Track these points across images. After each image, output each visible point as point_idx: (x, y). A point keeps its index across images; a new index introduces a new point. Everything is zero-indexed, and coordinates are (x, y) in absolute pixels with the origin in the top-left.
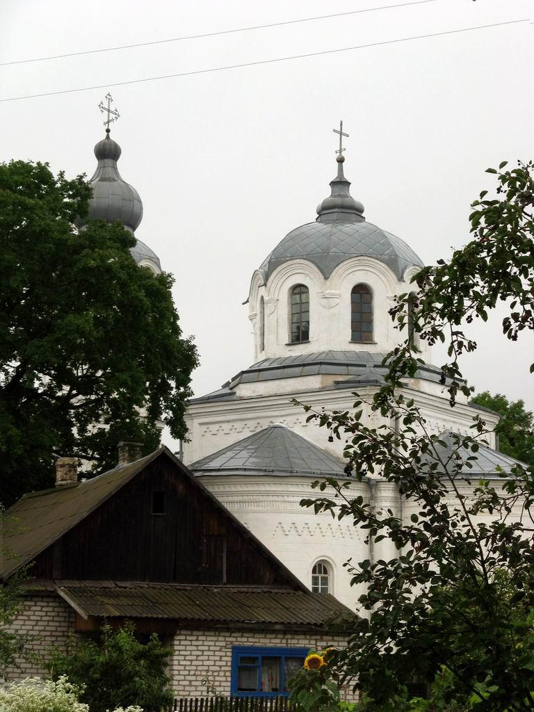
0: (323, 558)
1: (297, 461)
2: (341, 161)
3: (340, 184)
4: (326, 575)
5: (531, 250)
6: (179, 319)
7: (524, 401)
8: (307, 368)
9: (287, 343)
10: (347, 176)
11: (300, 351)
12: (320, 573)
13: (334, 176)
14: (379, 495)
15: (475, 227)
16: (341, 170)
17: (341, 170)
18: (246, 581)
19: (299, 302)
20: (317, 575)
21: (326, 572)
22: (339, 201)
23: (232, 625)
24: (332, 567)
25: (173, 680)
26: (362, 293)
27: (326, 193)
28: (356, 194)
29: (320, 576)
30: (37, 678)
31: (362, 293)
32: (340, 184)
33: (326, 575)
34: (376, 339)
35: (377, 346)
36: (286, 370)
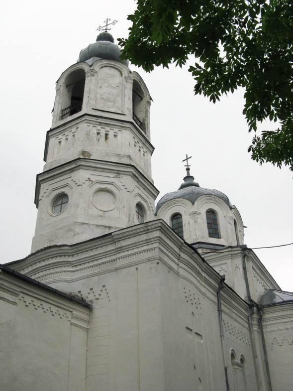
2: (188, 169)
3: (189, 177)
16: (188, 173)
17: (188, 173)
32: (189, 177)
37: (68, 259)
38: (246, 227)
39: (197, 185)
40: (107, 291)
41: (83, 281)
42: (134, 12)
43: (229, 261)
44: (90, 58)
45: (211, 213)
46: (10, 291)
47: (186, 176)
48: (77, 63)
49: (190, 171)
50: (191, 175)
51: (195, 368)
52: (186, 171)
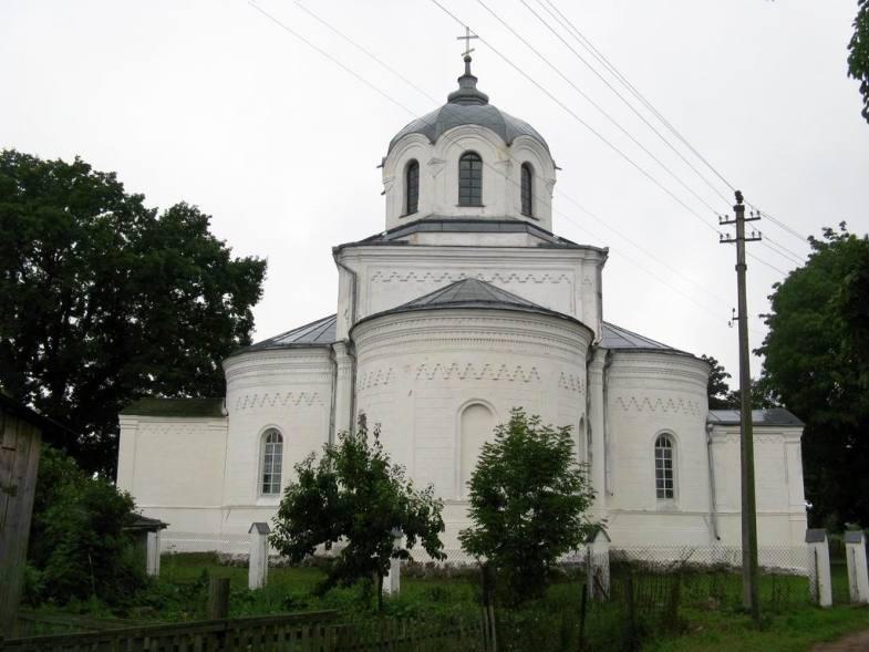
2: (468, 60)
3: (467, 79)
5: (53, 395)
6: (443, 530)
10: (473, 73)
11: (413, 218)
12: (664, 445)
13: (462, 72)
15: (715, 640)
16: (468, 68)
17: (468, 68)
18: (161, 562)
21: (669, 445)
22: (466, 92)
26: (471, 160)
27: (455, 87)
28: (481, 87)
30: (316, 465)
31: (471, 160)
32: (467, 79)
34: (484, 203)
35: (485, 209)
39: (483, 100)
43: (578, 267)
45: (527, 169)
49: (471, 64)
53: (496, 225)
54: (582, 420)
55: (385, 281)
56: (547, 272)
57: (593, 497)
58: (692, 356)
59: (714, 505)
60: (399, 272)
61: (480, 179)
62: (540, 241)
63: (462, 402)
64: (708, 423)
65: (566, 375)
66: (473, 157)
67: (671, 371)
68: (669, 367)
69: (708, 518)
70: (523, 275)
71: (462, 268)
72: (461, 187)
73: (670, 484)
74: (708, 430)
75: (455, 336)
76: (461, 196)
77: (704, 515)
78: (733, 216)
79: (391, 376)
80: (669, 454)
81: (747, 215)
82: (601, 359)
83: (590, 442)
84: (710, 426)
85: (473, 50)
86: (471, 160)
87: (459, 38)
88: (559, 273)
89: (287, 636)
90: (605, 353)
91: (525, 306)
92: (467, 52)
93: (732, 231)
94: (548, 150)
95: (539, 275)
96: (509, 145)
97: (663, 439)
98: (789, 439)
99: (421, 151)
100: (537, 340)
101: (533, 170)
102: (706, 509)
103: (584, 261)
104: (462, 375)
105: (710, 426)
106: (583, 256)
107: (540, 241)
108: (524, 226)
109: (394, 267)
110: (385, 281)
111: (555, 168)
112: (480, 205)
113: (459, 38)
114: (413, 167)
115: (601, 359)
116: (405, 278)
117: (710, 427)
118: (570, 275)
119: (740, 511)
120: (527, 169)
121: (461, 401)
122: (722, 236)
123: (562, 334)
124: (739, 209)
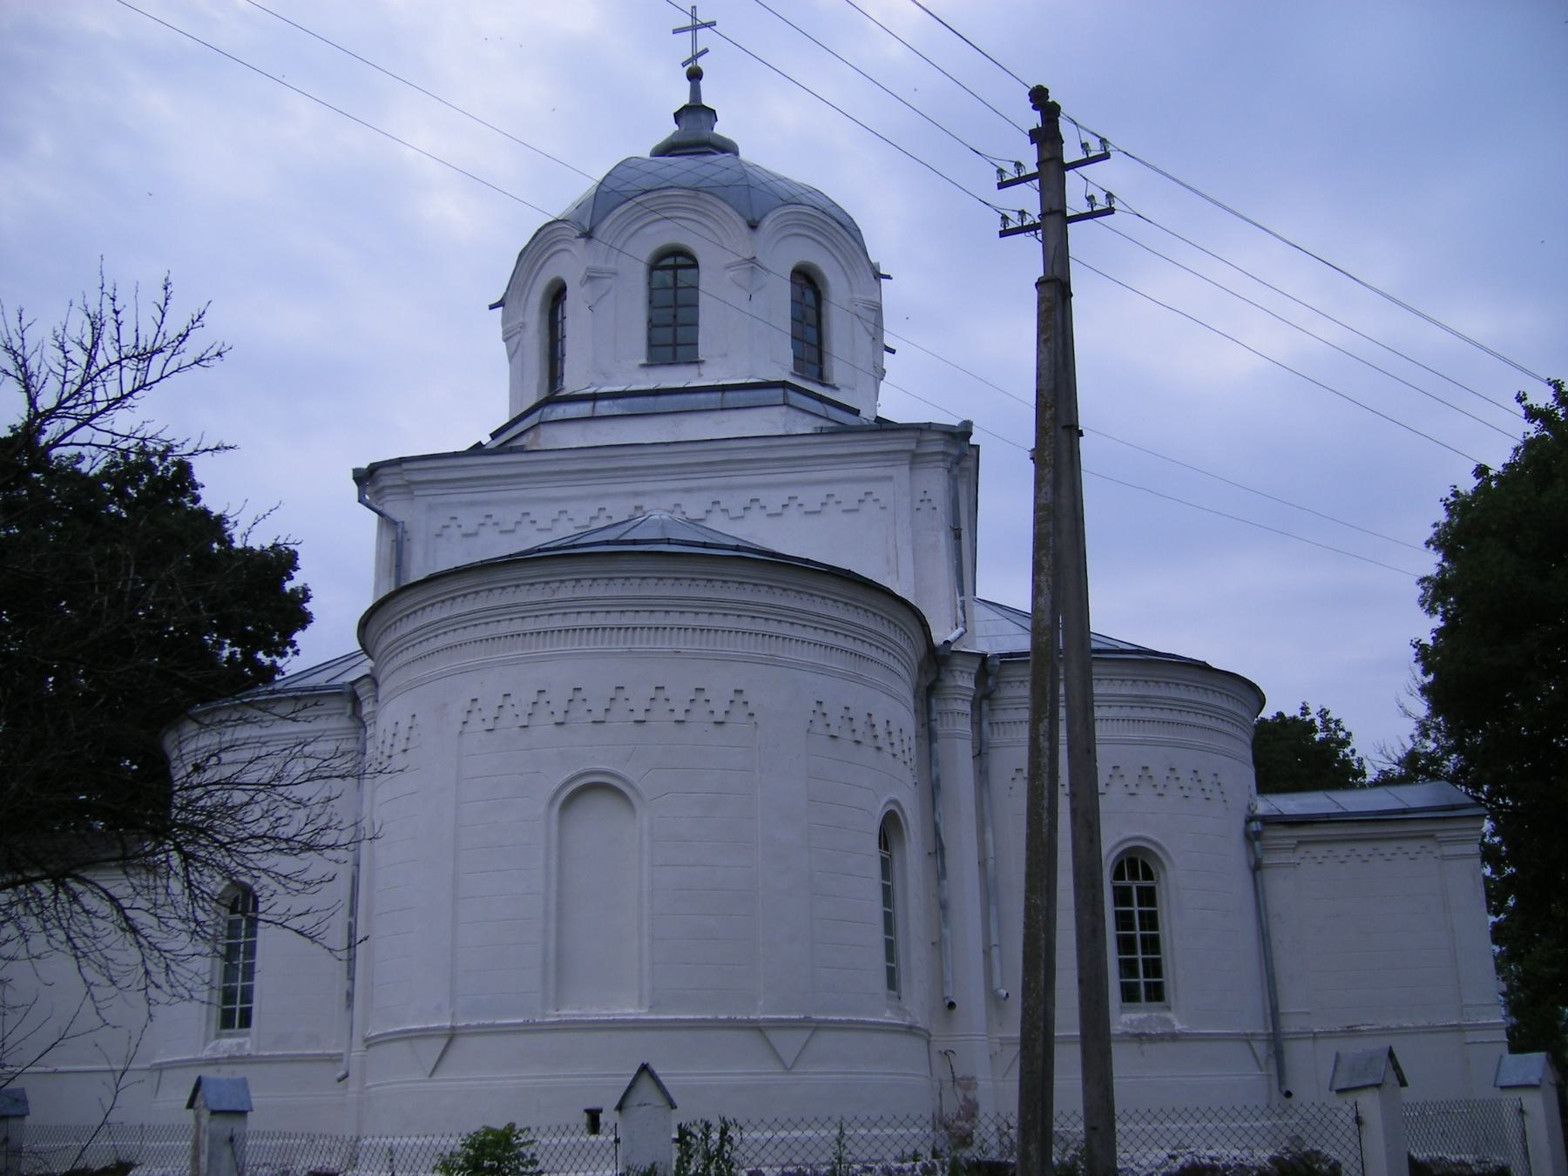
0: (1126, 846)
1: (625, 188)
2: (695, 76)
3: (695, 112)
4: (1148, 883)
7: (309, 586)
8: (729, 395)
9: (644, 361)
10: (706, 101)
12: (1134, 876)
13: (685, 100)
14: (949, 682)
16: (695, 92)
17: (695, 92)
19: (670, 350)
20: (1127, 882)
21: (1148, 875)
23: (220, 1061)
24: (1157, 857)
25: (148, 874)
29: (1134, 885)
32: (695, 112)
33: (1148, 883)
36: (651, 386)
37: (577, 620)
38: (893, 351)
39: (726, 147)
40: (750, 709)
41: (536, 448)
42: (216, 511)
43: (901, 472)
44: (414, 583)
45: (807, 281)
46: (510, 1031)
47: (686, 101)
48: (478, 449)
49: (704, 84)
50: (706, 102)
51: (901, 730)
52: (688, 84)
53: (716, 396)
54: (890, 829)
55: (466, 535)
56: (829, 489)
57: (142, 1126)
58: (1204, 667)
59: (1274, 1014)
60: (497, 513)
61: (694, 305)
62: (821, 423)
63: (561, 780)
64: (1250, 819)
65: (879, 721)
66: (680, 260)
67: (1143, 701)
68: (1140, 690)
69: (1261, 1048)
70: (775, 499)
71: (636, 494)
72: (652, 325)
73: (1154, 968)
74: (1251, 838)
75: (544, 623)
76: (652, 345)
77: (1247, 1039)
78: (1030, 158)
79: (414, 732)
80: (1148, 896)
81: (1071, 153)
82: (963, 681)
83: (941, 874)
84: (1255, 826)
85: (706, 51)
86: (675, 268)
87: (675, 32)
88: (858, 490)
89: (833, 1148)
90: (976, 664)
91: (1122, 651)
92: (695, 57)
93: (1028, 199)
94: (861, 234)
95: (813, 497)
96: (753, 226)
97: (1133, 862)
98: (1448, 850)
99: (570, 265)
100: (688, 620)
101: (824, 281)
102: (1254, 1024)
103: (915, 459)
104: (559, 717)
105: (1255, 826)
106: (913, 446)
107: (821, 423)
108: (780, 392)
109: (487, 503)
110: (466, 535)
111: (879, 276)
112: (695, 361)
113: (675, 32)
114: (557, 294)
115: (963, 681)
116: (510, 526)
117: (1258, 830)
118: (879, 490)
119: (1114, 1080)
120: (807, 281)
121: (556, 778)
122: (1005, 218)
123: (835, 613)
124: (1047, 136)
